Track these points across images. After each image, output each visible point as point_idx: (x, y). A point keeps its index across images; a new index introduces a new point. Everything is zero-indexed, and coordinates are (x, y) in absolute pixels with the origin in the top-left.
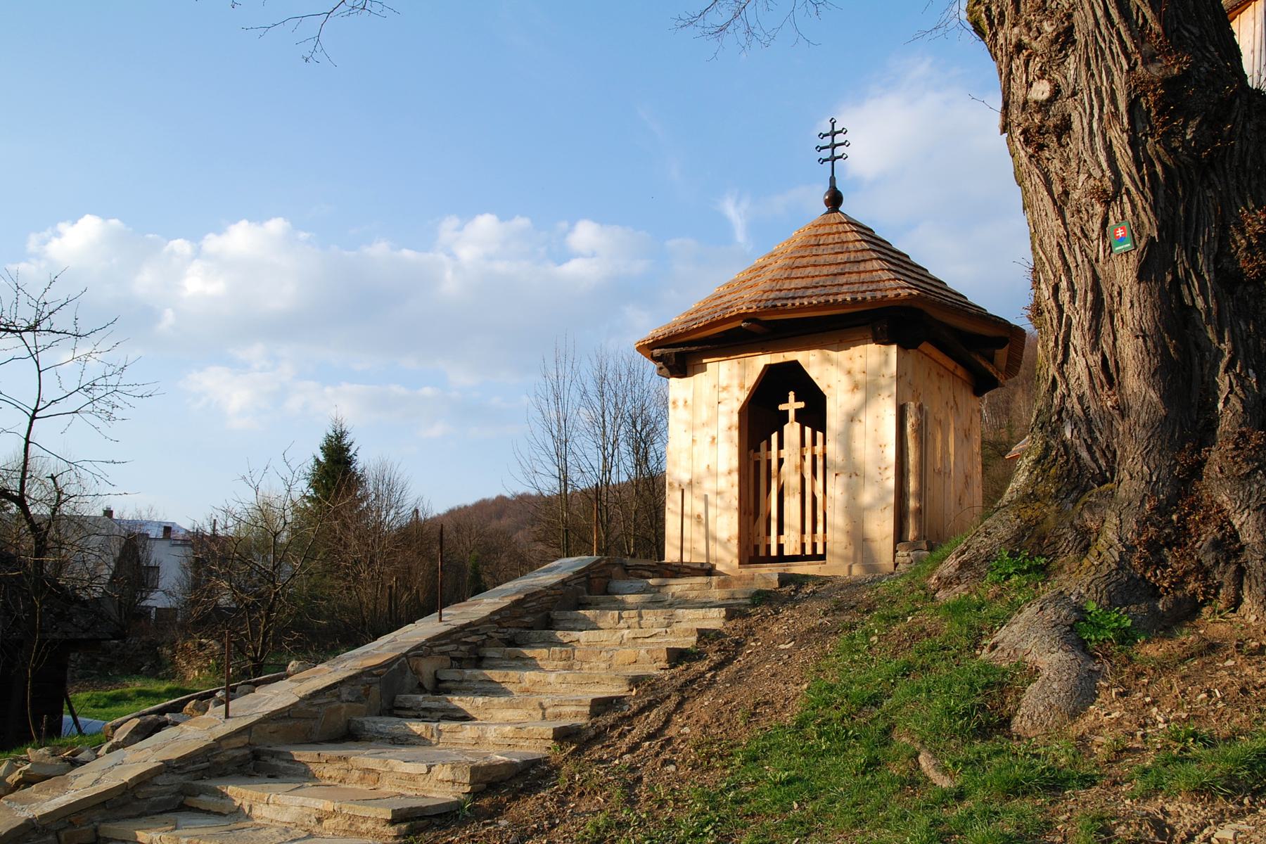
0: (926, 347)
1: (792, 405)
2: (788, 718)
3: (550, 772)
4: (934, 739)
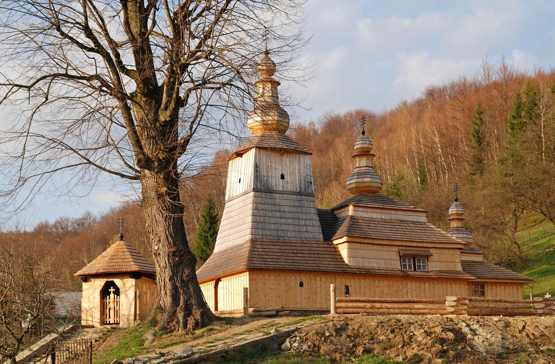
0: (143, 277)
1: (112, 290)
2: (116, 346)
3: (504, 67)
4: (134, 347)
